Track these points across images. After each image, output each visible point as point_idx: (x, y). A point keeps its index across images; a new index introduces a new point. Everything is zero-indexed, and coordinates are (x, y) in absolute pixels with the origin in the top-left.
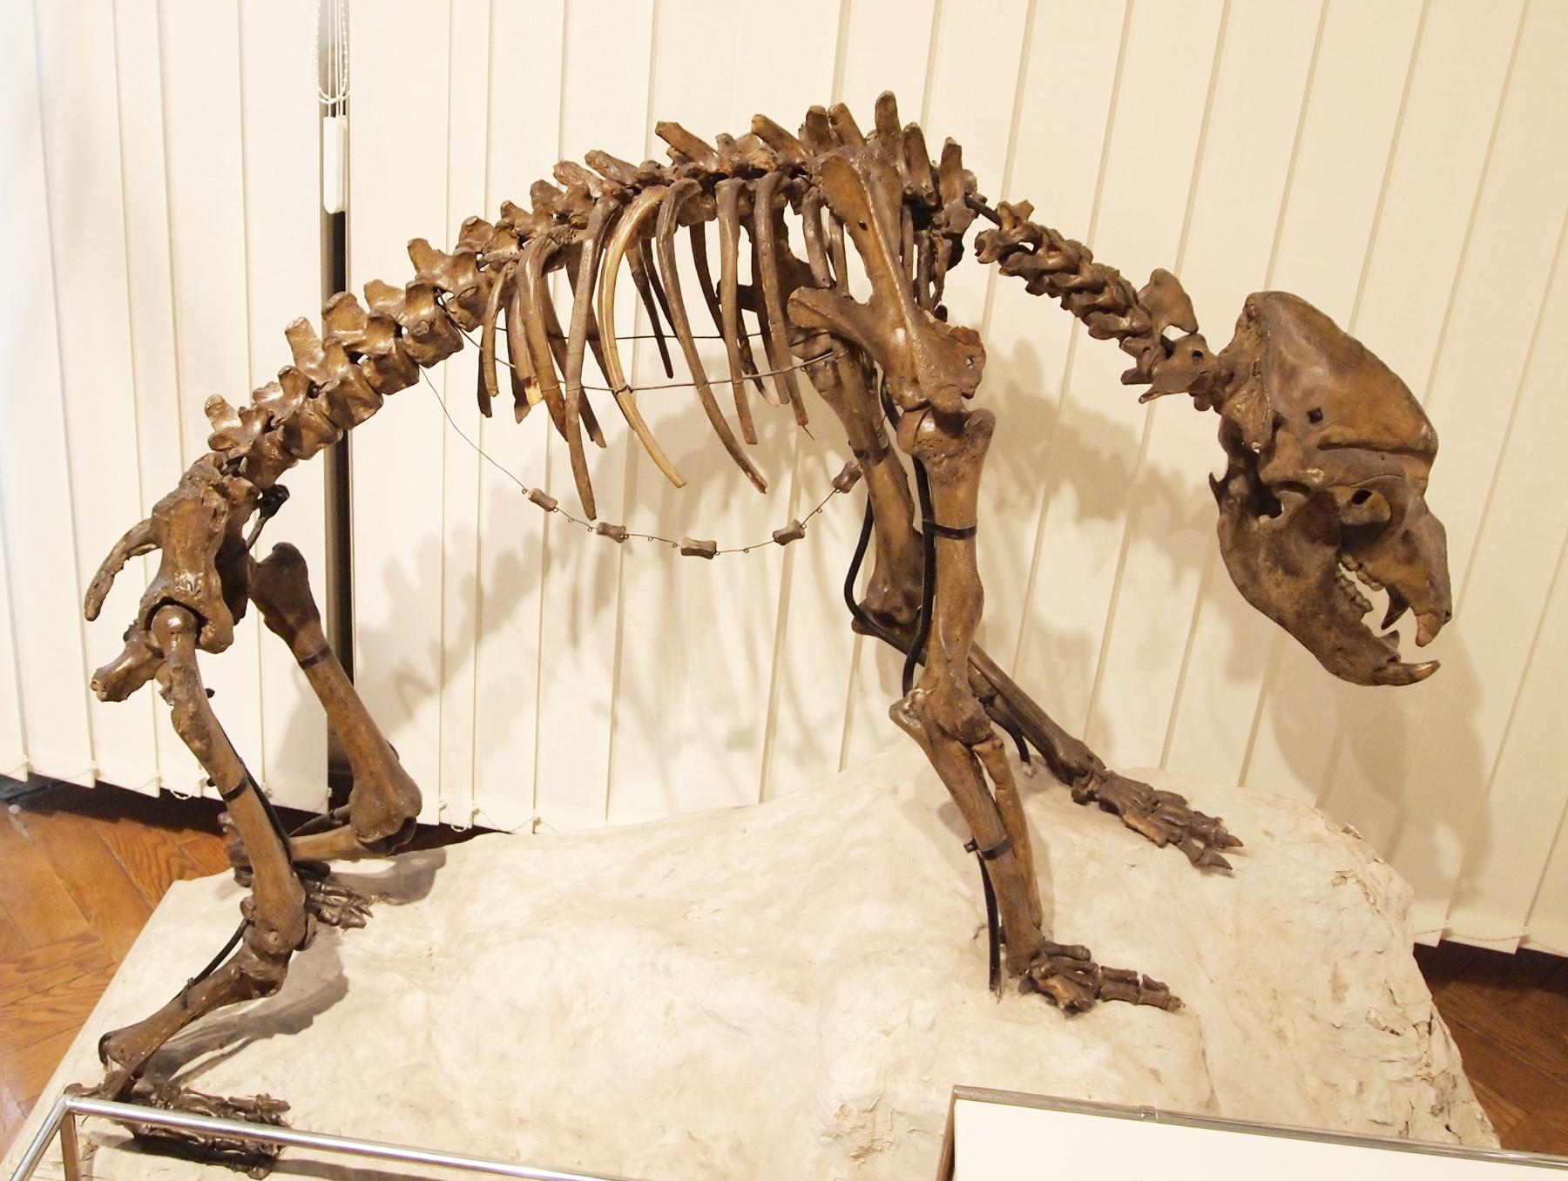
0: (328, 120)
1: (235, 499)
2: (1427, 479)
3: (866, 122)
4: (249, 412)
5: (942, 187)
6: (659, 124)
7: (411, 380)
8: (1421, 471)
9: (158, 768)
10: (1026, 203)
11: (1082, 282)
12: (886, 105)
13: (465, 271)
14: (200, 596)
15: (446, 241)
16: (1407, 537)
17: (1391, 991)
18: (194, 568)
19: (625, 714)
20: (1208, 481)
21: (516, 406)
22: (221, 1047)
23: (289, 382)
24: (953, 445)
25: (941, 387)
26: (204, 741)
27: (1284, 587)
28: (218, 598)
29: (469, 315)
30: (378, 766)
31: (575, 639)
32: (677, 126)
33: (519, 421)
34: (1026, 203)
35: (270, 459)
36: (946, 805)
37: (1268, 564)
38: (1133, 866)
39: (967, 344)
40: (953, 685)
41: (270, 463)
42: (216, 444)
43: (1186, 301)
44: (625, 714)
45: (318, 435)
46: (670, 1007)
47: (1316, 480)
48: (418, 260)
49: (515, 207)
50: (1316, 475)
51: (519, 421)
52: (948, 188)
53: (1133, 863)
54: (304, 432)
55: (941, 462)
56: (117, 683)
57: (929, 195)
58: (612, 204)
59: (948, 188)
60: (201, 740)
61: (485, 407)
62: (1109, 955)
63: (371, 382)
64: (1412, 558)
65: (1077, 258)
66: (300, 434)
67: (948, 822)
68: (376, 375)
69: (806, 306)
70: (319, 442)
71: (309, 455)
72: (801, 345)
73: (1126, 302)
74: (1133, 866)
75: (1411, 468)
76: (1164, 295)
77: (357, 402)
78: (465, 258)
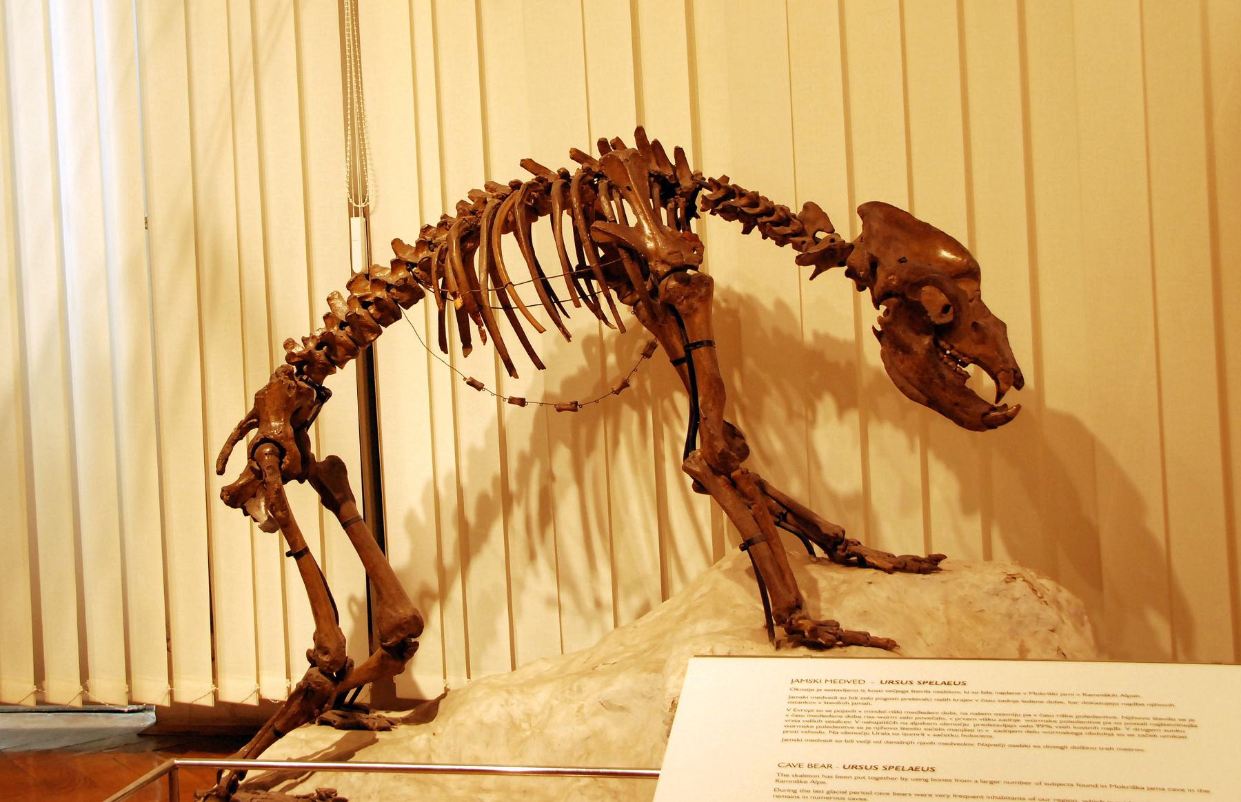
0: (354, 219)
1: (301, 389)
2: (980, 290)
3: (631, 143)
4: (307, 339)
5: (678, 174)
6: (522, 160)
7: (397, 317)
8: (975, 286)
9: (258, 682)
10: (724, 176)
11: (761, 211)
12: (640, 133)
13: (423, 251)
14: (282, 434)
15: (411, 237)
16: (975, 326)
17: (1064, 654)
18: (278, 419)
19: (566, 599)
20: (872, 330)
21: (463, 347)
22: (296, 779)
23: (329, 321)
24: (687, 291)
25: (670, 253)
26: (284, 512)
27: (906, 363)
28: (292, 439)
29: (426, 275)
30: (393, 591)
31: (532, 556)
32: (531, 160)
33: (465, 356)
34: (724, 176)
35: (320, 363)
36: (750, 568)
37: (892, 349)
38: (870, 583)
39: (690, 241)
40: (709, 432)
41: (319, 366)
42: (290, 360)
43: (825, 216)
44: (566, 599)
45: (346, 349)
46: (580, 708)
47: (894, 283)
48: (398, 250)
49: (448, 216)
50: (893, 280)
51: (465, 356)
52: (681, 174)
53: (870, 581)
54: (338, 347)
55: (683, 301)
56: (235, 493)
57: (671, 177)
58: (497, 201)
59: (681, 174)
60: (282, 511)
61: (443, 346)
62: (849, 624)
63: (374, 316)
64: (983, 340)
65: (755, 200)
66: (336, 348)
67: (750, 575)
68: (376, 312)
69: (600, 230)
70: (347, 355)
71: (342, 364)
72: (629, 297)
73: (786, 218)
74: (870, 583)
75: (964, 286)
76: (811, 215)
77: (366, 329)
78: (421, 244)
